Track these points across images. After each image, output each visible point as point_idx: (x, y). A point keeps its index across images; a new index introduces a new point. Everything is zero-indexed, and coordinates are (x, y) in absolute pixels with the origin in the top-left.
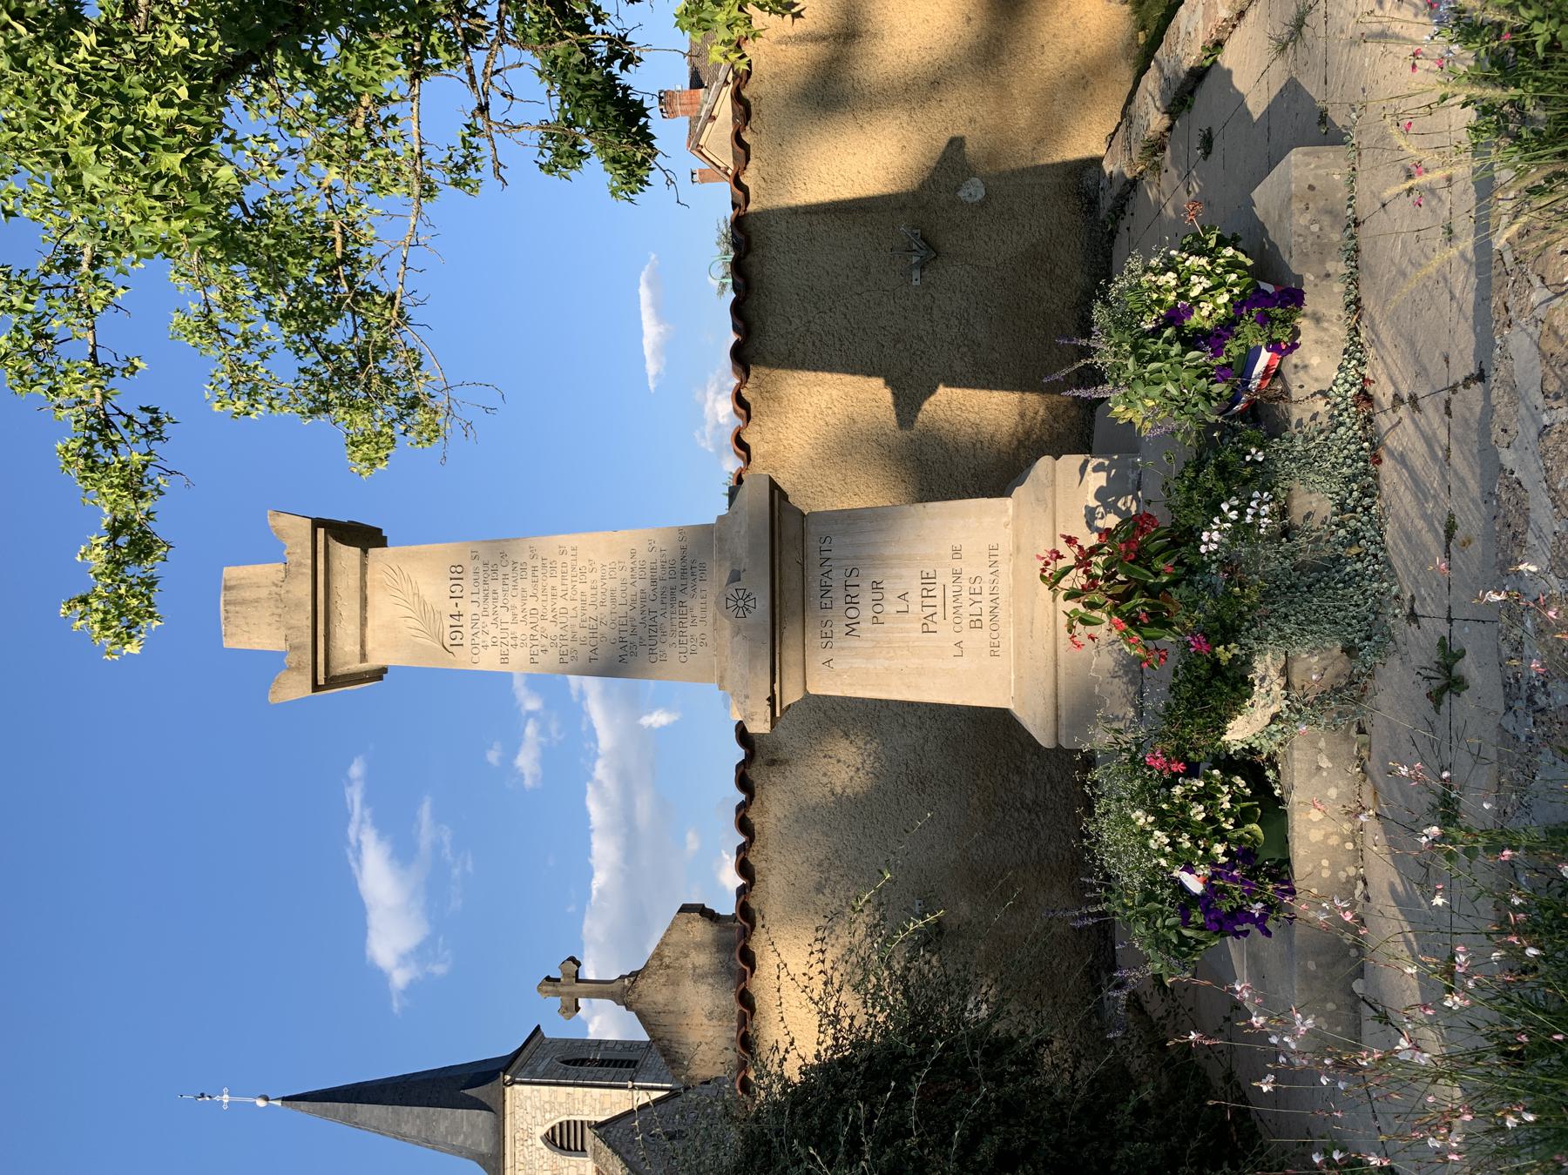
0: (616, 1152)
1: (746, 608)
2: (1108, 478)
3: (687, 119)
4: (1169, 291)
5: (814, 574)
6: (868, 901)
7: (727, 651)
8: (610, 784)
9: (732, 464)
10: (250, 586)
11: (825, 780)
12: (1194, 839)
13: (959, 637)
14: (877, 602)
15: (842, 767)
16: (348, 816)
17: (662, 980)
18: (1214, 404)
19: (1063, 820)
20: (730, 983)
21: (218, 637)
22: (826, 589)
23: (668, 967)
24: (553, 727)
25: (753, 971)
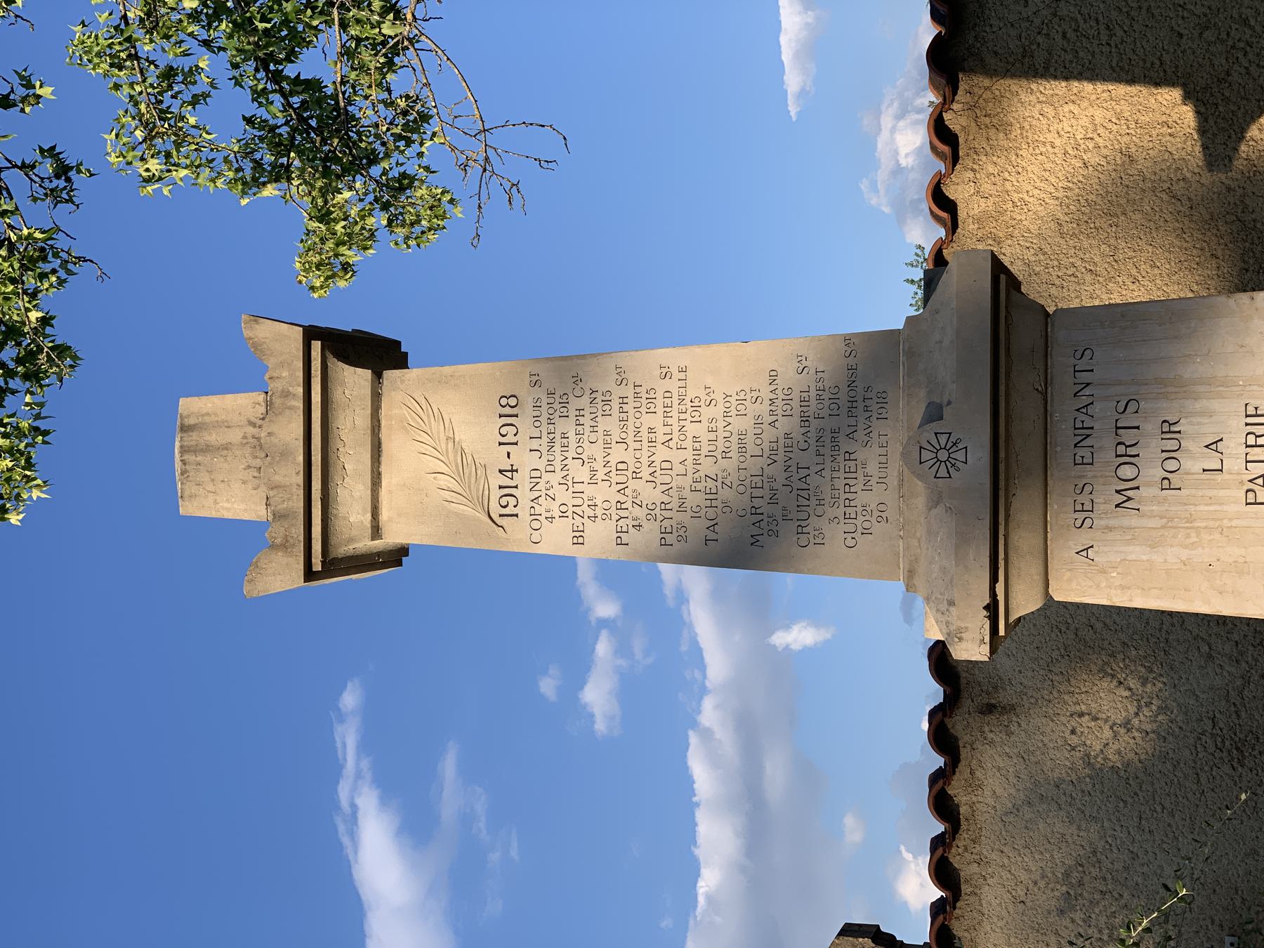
1: (951, 463)
6: (1147, 930)
7: (921, 532)
8: (724, 735)
9: (923, 233)
10: (218, 425)
11: (1074, 740)
14: (1170, 454)
15: (1106, 719)
21: (172, 498)
22: (1083, 433)
24: (638, 645)
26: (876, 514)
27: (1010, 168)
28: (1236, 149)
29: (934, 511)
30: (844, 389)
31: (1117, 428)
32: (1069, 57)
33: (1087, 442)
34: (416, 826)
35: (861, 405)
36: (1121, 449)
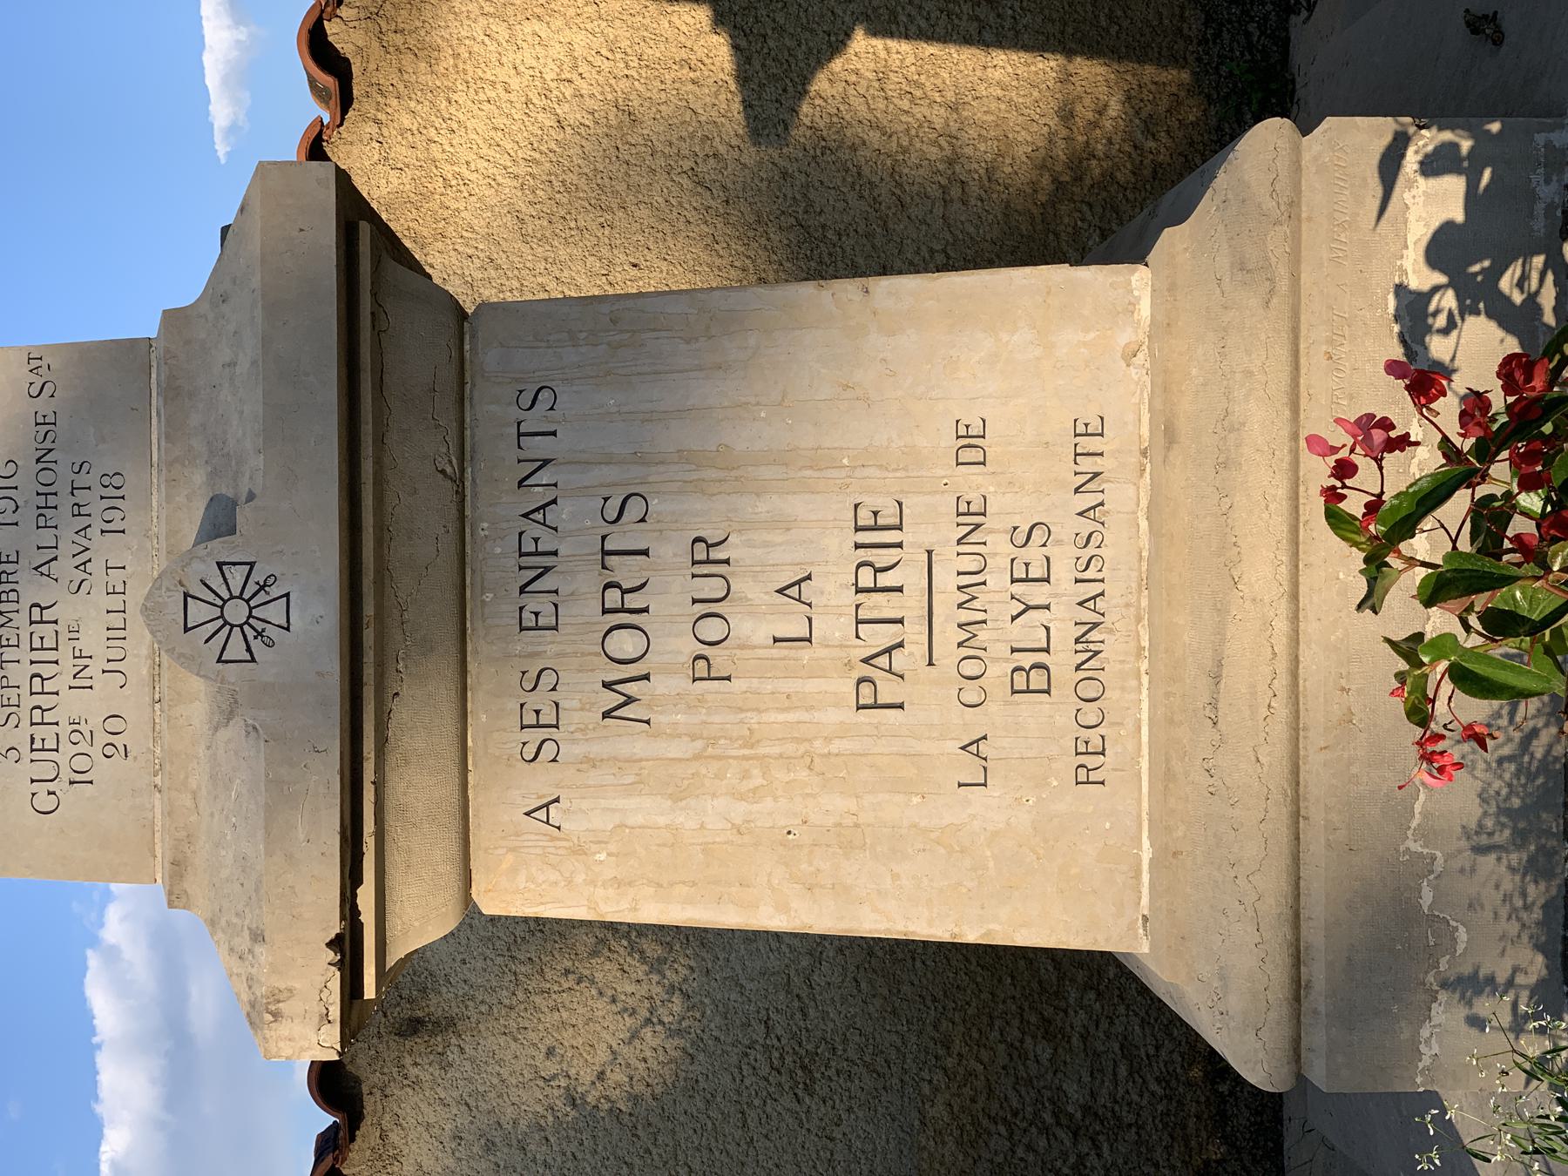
5: (498, 511)
11: (550, 1068)
13: (976, 724)
14: (709, 608)
19: (1159, 1155)
22: (537, 566)
26: (102, 738)
27: (438, 122)
28: (794, 111)
29: (224, 734)
30: (28, 465)
31: (605, 553)
33: (546, 583)
36: (613, 597)
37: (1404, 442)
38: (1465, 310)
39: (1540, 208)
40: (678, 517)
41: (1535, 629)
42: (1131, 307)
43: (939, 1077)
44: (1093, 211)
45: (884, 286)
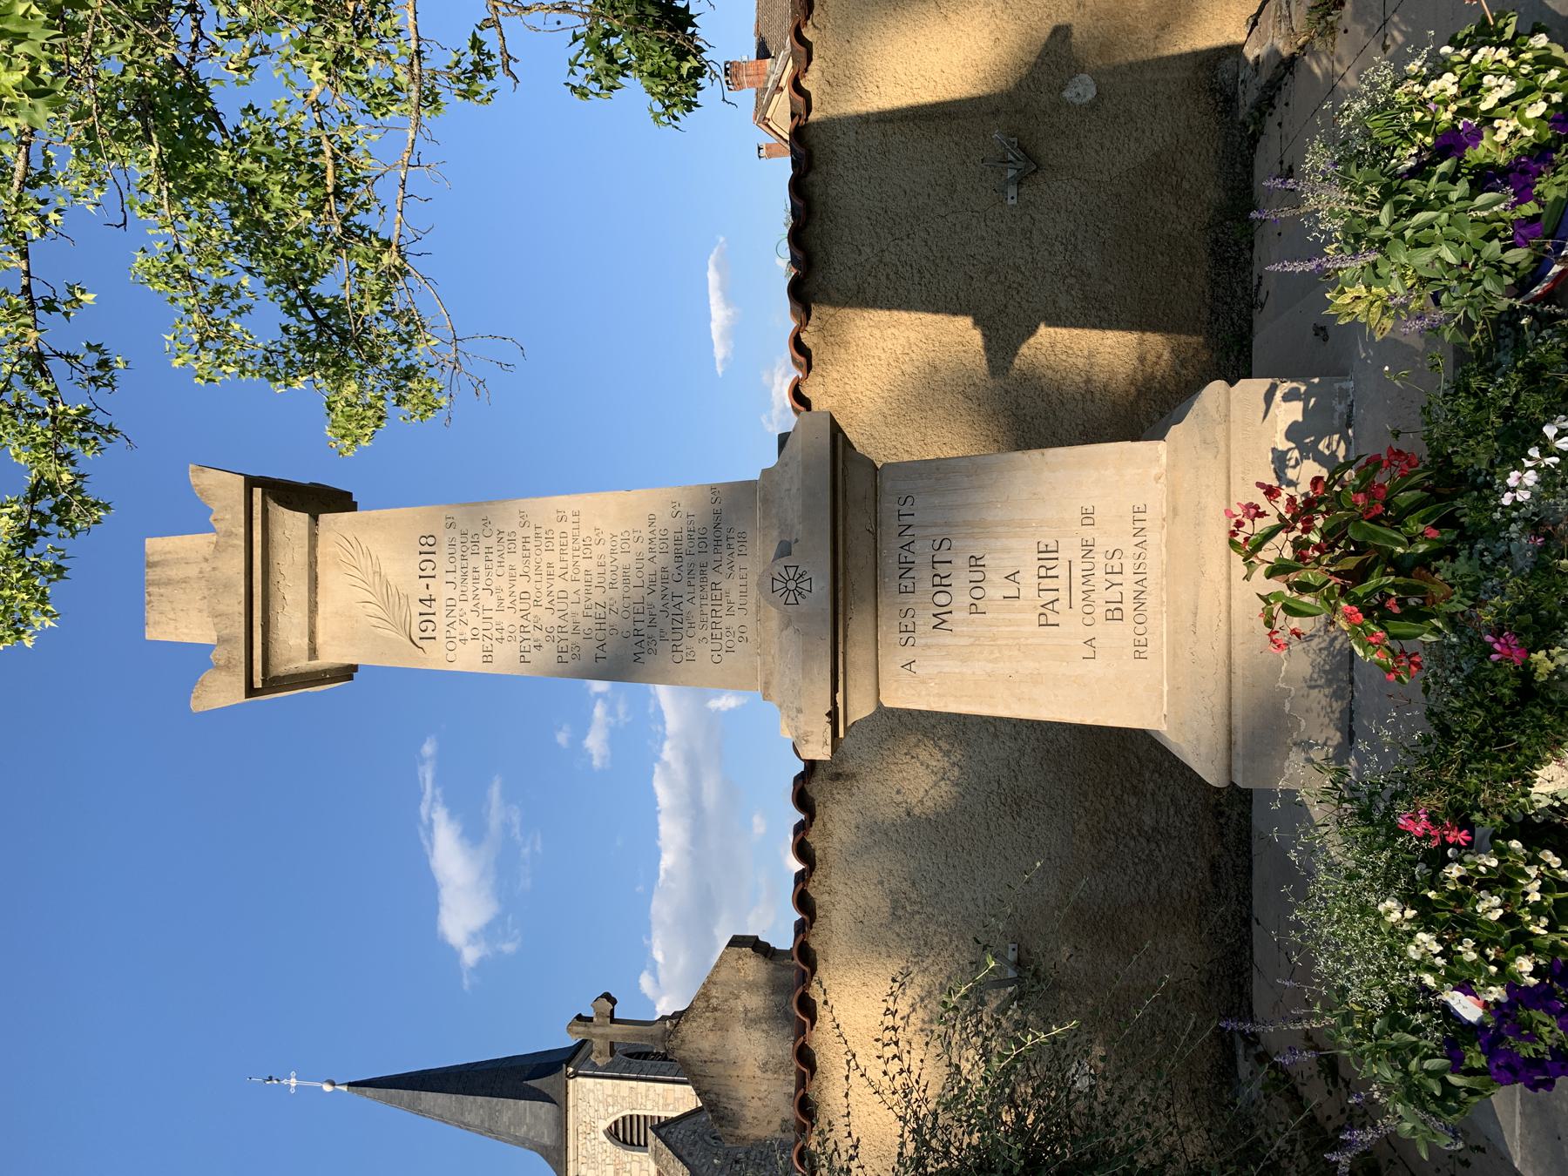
0: (680, 1158)
2: (1305, 411)
3: (754, 90)
4: (1445, 104)
6: (965, 997)
7: (774, 650)
8: (678, 767)
10: (178, 561)
11: (899, 798)
12: (1480, 948)
13: (1090, 633)
14: (977, 584)
15: (918, 782)
16: (421, 794)
17: (710, 1024)
18: (1509, 281)
19: (1190, 852)
20: (788, 1030)
21: (142, 624)
22: (907, 567)
23: (715, 1009)
24: (621, 709)
25: (813, 1023)
29: (785, 633)
32: (890, 293)
34: (473, 833)
35: (725, 544)
36: (937, 580)
37: (1262, 515)
38: (1304, 457)
39: (1336, 415)
40: (962, 549)
41: (1316, 589)
42: (1158, 459)
43: (1081, 811)
44: (1142, 413)
45: (1050, 452)
